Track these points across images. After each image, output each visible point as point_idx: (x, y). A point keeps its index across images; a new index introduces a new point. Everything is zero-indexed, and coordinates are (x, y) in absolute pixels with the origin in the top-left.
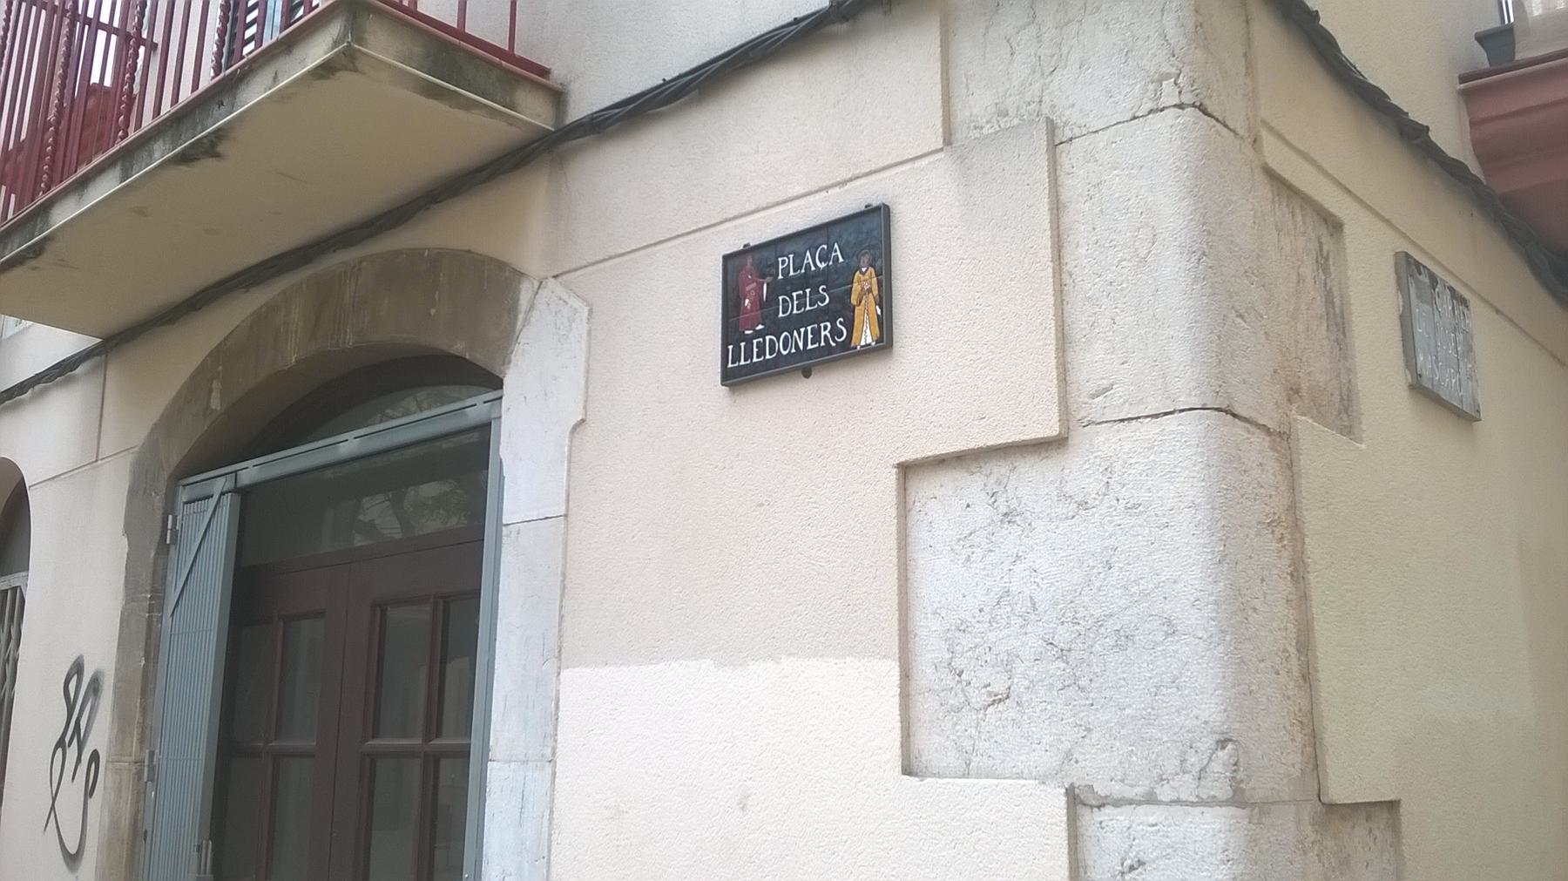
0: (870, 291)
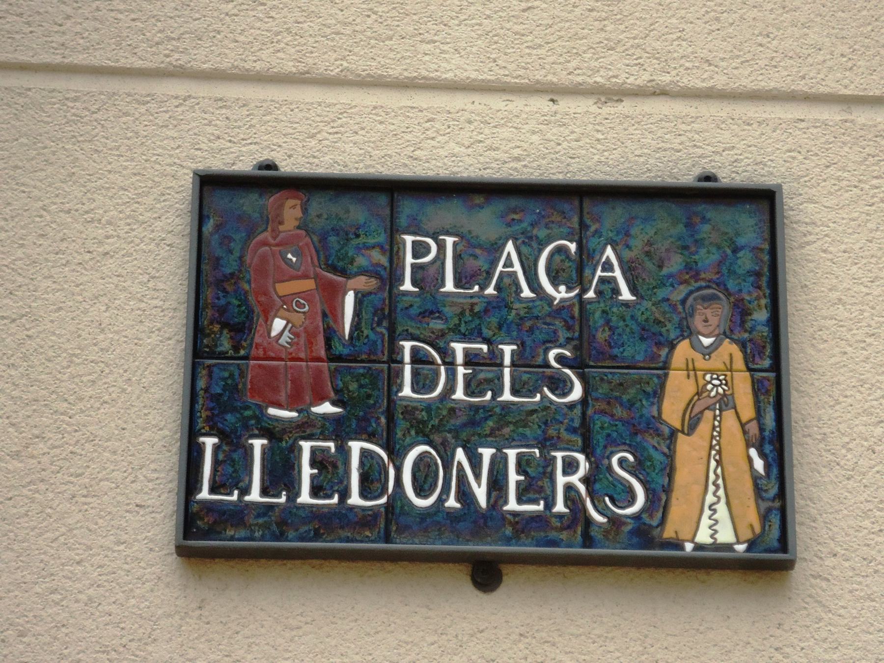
0: (726, 402)
